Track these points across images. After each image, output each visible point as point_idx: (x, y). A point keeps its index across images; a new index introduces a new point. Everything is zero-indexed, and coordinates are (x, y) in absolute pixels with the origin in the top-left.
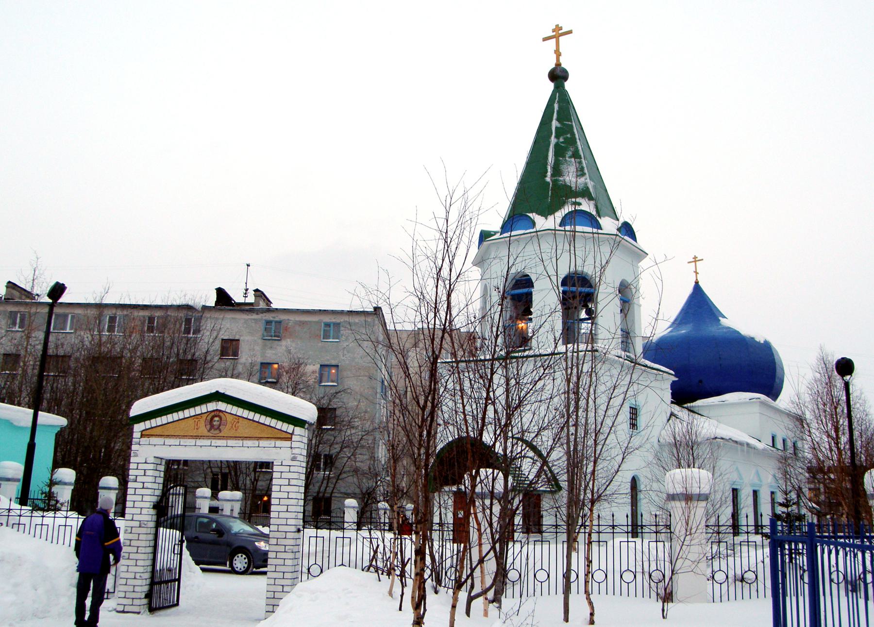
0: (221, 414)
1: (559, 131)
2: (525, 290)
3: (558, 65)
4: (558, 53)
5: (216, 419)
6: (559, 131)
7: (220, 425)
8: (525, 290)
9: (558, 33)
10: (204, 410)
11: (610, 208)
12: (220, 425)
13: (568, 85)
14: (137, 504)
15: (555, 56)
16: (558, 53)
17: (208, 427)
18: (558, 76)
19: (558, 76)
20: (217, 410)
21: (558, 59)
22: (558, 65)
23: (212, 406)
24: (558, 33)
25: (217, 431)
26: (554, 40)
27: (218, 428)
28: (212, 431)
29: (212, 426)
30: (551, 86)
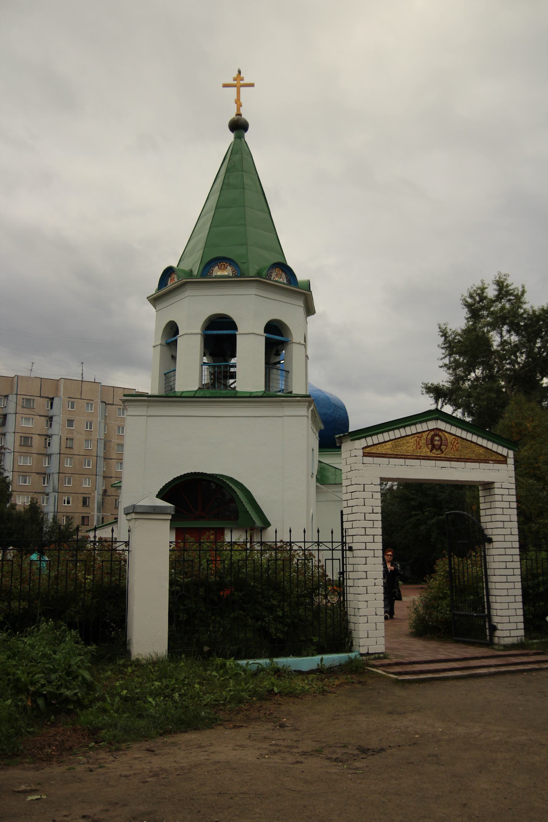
0: (440, 434)
1: (238, 187)
2: (209, 332)
4: (238, 102)
5: (437, 438)
6: (238, 187)
7: (441, 445)
8: (209, 332)
10: (425, 429)
11: (261, 192)
12: (441, 445)
13: (248, 136)
14: (370, 539)
15: (235, 106)
16: (238, 102)
17: (430, 446)
18: (239, 126)
20: (437, 429)
21: (238, 109)
22: (239, 115)
23: (432, 425)
25: (439, 452)
26: (235, 89)
27: (440, 448)
28: (434, 451)
29: (433, 447)
30: (230, 137)
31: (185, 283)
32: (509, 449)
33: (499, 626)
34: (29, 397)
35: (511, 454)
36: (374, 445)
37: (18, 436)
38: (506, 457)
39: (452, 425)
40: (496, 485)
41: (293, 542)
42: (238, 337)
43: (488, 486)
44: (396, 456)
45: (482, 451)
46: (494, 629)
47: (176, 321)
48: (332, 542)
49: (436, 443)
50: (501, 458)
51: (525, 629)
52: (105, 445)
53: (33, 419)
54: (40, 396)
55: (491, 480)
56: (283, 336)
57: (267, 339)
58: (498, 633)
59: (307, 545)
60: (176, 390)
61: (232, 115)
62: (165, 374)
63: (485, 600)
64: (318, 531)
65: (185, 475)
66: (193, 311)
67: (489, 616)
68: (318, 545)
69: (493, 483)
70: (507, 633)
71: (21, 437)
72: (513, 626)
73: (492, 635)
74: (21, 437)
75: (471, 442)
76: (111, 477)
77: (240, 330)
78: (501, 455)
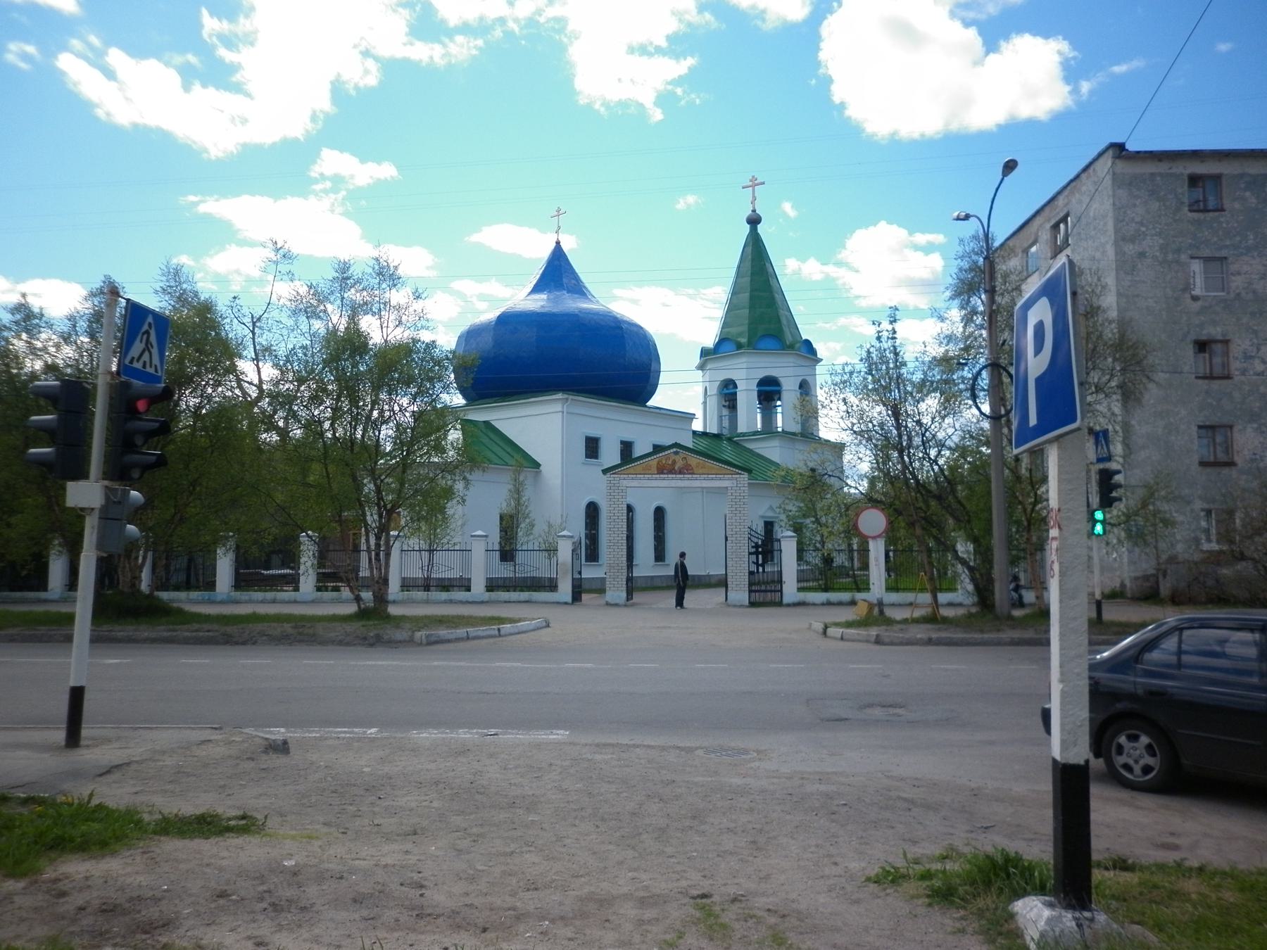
3: (754, 211)
4: (754, 198)
9: (754, 184)
18: (754, 221)
19: (754, 221)
22: (754, 211)
24: (754, 184)
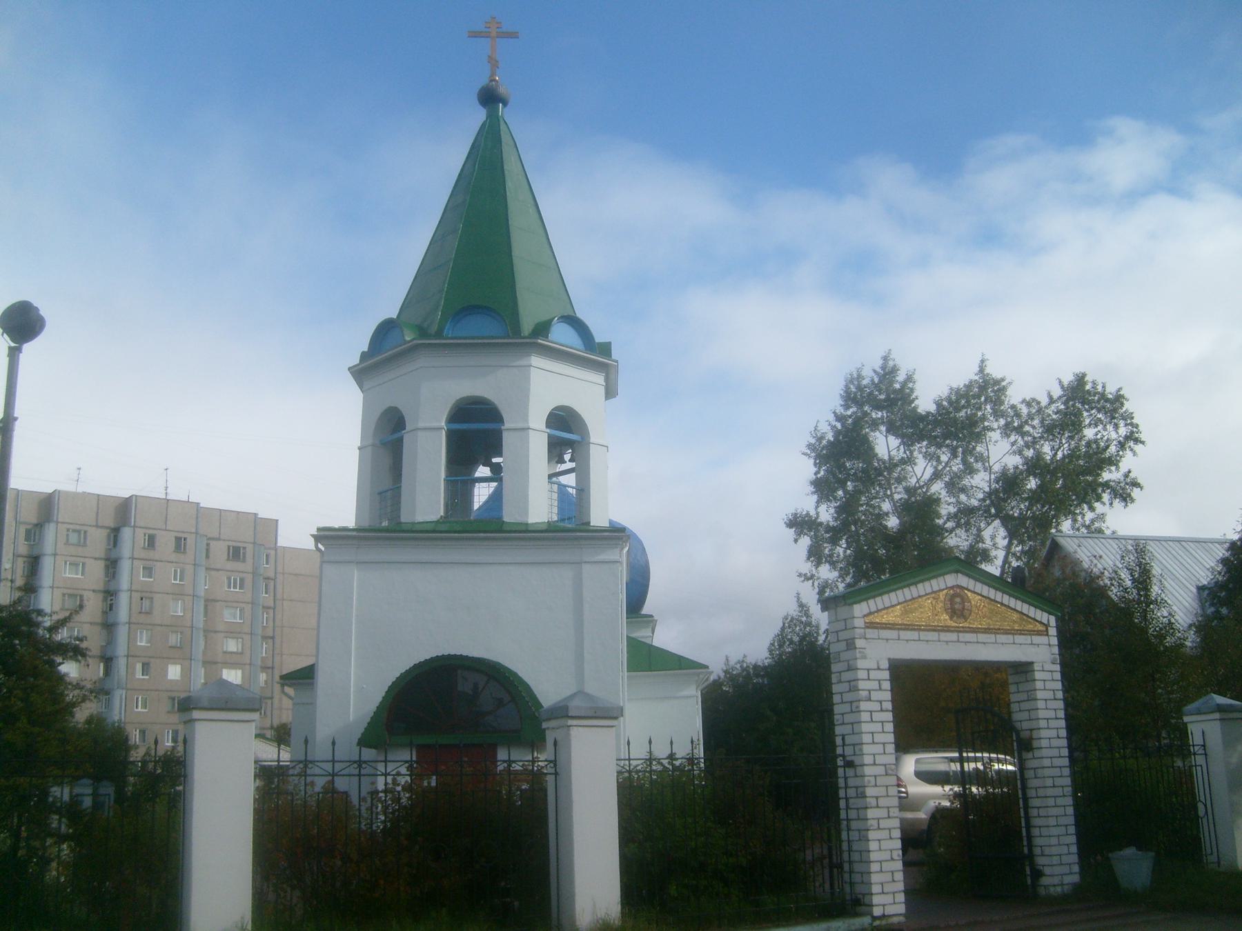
4: (493, 63)
5: (958, 600)
31: (415, 348)
32: (1050, 613)
33: (1047, 871)
34: (78, 527)
35: (1053, 620)
36: (878, 611)
37: (58, 593)
38: (1047, 626)
39: (976, 580)
40: (1036, 667)
41: (311, 762)
42: (505, 435)
43: (1023, 669)
44: (907, 627)
45: (1015, 616)
46: (1037, 874)
47: (385, 407)
48: (333, 761)
49: (957, 606)
50: (1041, 628)
51: (1080, 873)
52: (206, 606)
53: (84, 564)
54: (97, 526)
55: (1029, 660)
56: (570, 431)
57: (550, 436)
58: (1045, 881)
59: (338, 766)
60: (403, 520)
61: (484, 81)
62: (380, 493)
63: (1024, 834)
64: (629, 743)
65: (432, 660)
66: (433, 394)
67: (1031, 856)
68: (360, 766)
69: (1032, 663)
70: (1056, 880)
71: (64, 595)
72: (1066, 869)
73: (1035, 885)
74: (64, 595)
75: (1002, 604)
76: (216, 663)
77: (507, 425)
78: (1041, 623)
